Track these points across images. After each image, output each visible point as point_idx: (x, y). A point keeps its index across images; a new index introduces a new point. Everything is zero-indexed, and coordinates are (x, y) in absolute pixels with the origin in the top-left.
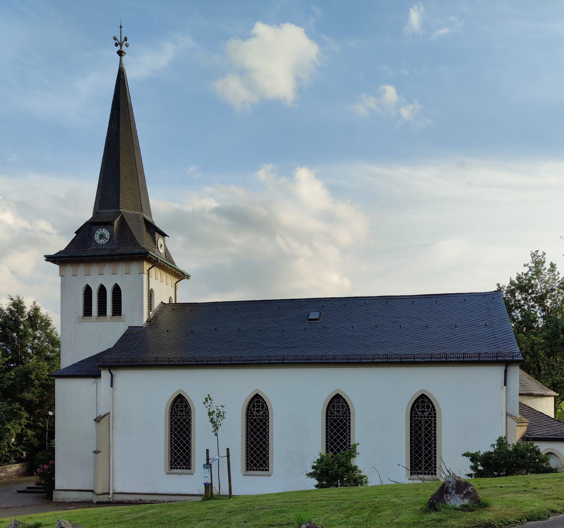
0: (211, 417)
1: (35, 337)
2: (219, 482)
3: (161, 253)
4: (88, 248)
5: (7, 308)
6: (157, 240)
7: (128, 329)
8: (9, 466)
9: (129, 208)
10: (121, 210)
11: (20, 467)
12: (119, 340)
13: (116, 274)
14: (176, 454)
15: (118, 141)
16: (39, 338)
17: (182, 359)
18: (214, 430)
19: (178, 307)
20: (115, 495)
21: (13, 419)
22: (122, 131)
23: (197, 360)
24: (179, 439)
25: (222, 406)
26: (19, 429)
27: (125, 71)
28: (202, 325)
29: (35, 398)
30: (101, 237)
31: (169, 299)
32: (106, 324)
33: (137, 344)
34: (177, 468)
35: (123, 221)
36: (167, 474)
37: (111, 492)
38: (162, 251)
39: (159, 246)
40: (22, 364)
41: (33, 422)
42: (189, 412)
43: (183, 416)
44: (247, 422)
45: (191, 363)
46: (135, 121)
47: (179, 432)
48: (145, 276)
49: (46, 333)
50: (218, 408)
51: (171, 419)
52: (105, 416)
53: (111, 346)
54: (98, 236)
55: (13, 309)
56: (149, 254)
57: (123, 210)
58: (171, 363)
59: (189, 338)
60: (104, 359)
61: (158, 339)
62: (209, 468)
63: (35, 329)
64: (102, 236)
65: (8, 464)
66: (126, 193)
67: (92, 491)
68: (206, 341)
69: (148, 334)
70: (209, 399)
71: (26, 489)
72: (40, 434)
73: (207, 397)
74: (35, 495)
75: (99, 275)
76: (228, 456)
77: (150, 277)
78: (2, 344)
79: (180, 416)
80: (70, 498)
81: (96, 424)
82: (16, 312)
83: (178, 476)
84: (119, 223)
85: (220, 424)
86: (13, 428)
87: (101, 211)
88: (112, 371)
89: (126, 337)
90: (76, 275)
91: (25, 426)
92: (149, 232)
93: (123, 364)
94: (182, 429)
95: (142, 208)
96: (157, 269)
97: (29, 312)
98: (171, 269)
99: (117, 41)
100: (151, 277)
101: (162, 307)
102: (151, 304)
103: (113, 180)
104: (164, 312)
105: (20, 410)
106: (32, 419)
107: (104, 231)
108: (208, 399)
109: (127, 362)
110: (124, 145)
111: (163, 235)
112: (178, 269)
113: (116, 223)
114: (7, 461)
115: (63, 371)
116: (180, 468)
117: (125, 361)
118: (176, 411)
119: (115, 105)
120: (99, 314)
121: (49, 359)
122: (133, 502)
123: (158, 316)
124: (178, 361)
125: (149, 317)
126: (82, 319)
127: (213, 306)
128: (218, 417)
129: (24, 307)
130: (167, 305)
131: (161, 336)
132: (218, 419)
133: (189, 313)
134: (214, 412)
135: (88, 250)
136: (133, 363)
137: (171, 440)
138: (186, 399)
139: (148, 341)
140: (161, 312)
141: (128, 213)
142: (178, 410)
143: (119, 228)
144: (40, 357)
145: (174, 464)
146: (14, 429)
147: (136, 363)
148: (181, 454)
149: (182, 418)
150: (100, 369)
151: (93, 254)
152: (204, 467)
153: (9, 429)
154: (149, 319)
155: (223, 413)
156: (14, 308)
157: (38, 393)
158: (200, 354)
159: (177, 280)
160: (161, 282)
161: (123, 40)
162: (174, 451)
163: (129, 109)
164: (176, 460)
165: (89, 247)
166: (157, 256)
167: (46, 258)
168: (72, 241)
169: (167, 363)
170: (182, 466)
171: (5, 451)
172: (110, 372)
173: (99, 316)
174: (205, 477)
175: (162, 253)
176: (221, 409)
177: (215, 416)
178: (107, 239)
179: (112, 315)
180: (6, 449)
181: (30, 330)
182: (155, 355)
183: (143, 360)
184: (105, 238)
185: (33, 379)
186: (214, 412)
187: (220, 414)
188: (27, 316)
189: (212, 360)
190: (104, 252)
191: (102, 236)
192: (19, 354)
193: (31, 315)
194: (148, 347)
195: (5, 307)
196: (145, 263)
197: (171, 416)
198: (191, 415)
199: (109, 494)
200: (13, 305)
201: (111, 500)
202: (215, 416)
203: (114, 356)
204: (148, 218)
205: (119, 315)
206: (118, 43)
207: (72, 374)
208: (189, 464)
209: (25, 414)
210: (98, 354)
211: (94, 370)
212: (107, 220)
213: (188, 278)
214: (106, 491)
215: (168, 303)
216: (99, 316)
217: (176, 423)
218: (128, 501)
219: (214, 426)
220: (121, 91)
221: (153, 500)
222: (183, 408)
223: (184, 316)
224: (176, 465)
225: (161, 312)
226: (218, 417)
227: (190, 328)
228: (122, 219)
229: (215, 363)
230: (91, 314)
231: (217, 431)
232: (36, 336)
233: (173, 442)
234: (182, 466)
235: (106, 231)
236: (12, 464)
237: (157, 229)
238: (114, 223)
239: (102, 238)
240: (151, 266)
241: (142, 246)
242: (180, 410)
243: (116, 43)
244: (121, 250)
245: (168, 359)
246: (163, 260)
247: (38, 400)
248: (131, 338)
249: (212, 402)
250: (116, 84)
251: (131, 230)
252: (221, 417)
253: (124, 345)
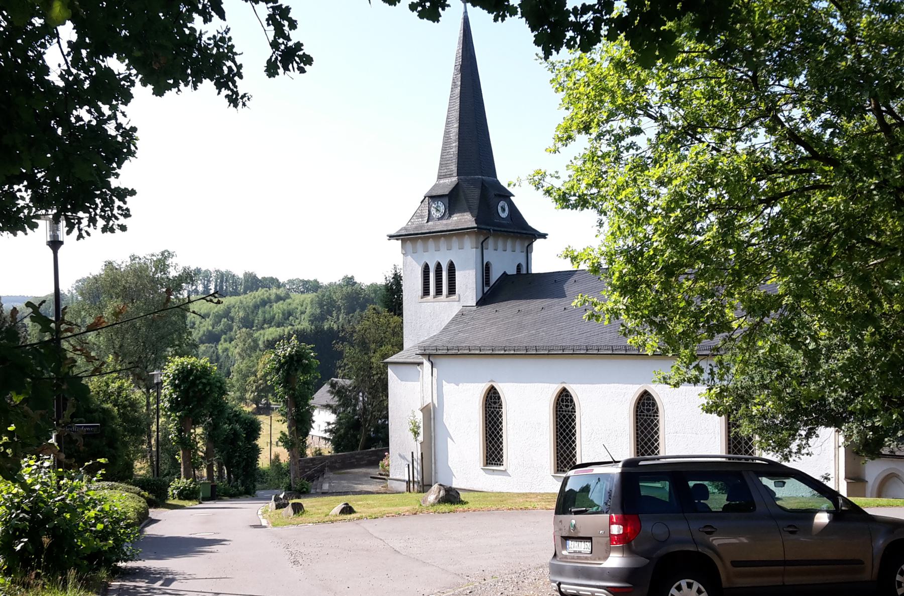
44: (557, 418)
164: (491, 455)
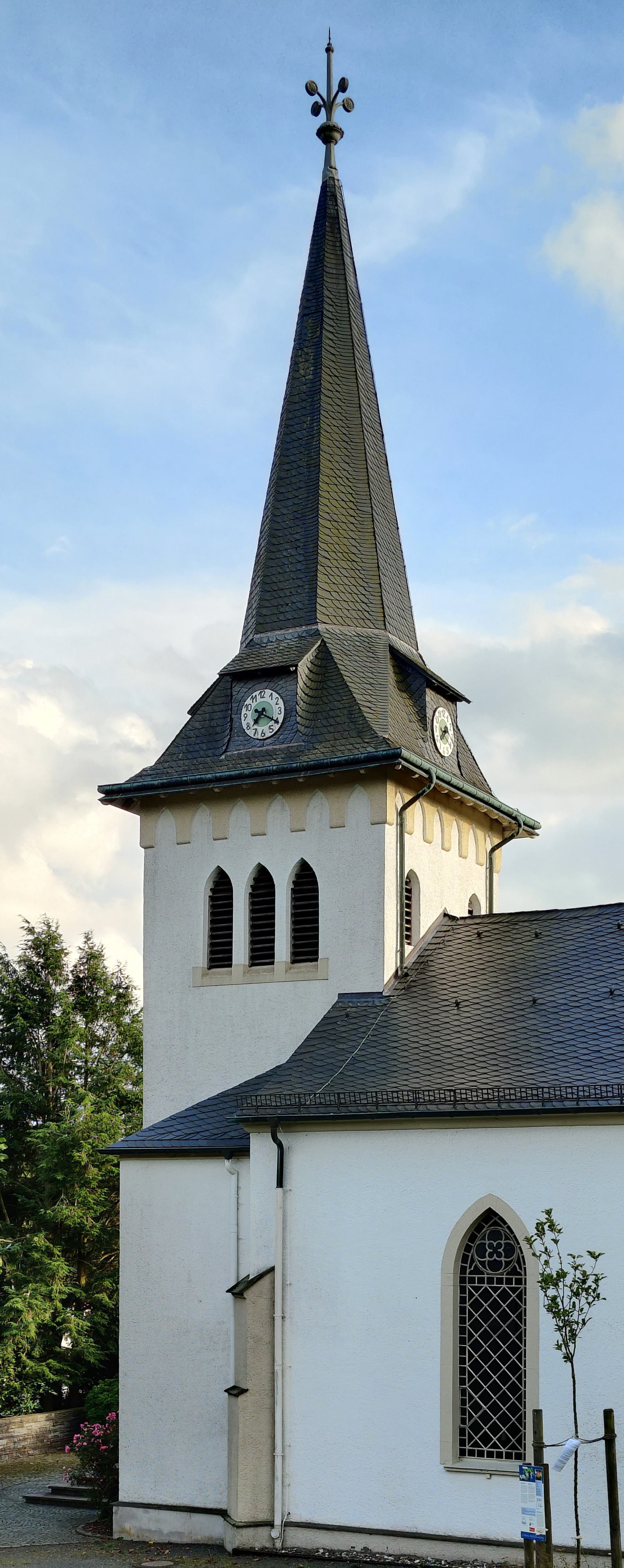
0: (551, 1292)
1: (92, 1041)
2: (578, 1534)
3: (442, 757)
4: (221, 755)
5: (20, 957)
6: (429, 713)
7: (337, 1002)
8: (17, 1419)
9: (347, 620)
10: (321, 627)
11: (48, 1423)
12: (308, 1039)
13: (304, 830)
14: (476, 1407)
15: (315, 412)
16: (103, 1043)
17: (496, 1094)
18: (561, 1342)
19: (496, 926)
20: (291, 1532)
21: (29, 1282)
22: (328, 378)
23: (546, 1096)
24: (486, 1357)
25: (594, 1256)
26: (45, 1310)
27: (340, 187)
28: (568, 982)
29: (90, 1219)
30: (259, 718)
31: (470, 903)
32: (272, 989)
33: (360, 1050)
34: (481, 1454)
35: (325, 658)
36: (449, 1470)
37: (278, 1522)
38: (446, 748)
39: (437, 733)
40: (59, 1119)
41: (86, 1292)
42: (520, 1268)
43: (500, 1281)
45: (525, 1106)
46: (370, 343)
47: (485, 1336)
48: (390, 832)
49: (118, 1026)
50: (579, 1261)
51: (463, 1290)
52: (260, 1277)
53: (284, 1059)
54: (249, 713)
55: (35, 959)
56: (400, 760)
57: (327, 626)
58: (460, 1108)
59: (524, 1025)
60: (259, 1098)
61: (426, 1031)
62: (539, 1479)
63: (92, 1016)
64: (261, 714)
65: (16, 1413)
66: (335, 570)
67: (223, 1513)
68: (580, 1034)
69: (396, 1016)
70: (549, 1226)
71: (49, 1494)
72: (104, 1325)
73: (543, 1218)
74: (70, 1512)
75: (253, 835)
76: (609, 1438)
77: (406, 836)
78: (7, 1061)
79: (490, 1281)
80: (160, 1532)
81: (235, 1303)
82: (42, 968)
83: (482, 1478)
84: (315, 670)
85: (583, 1320)
86: (29, 1307)
87: (262, 635)
88: (280, 1136)
89: (330, 1027)
90: (187, 840)
91: (62, 1301)
92: (403, 692)
93: (313, 1113)
94: (495, 1327)
95: (384, 616)
96: (432, 810)
97: (75, 966)
98: (475, 804)
99: (316, 98)
100: (411, 834)
101: (445, 928)
102: (408, 922)
103: (297, 537)
104: (450, 943)
105: (51, 1255)
106: (83, 1281)
107: (267, 699)
108: (546, 1227)
109: (327, 1106)
110: (334, 422)
111: (452, 697)
112: (496, 804)
113: (304, 668)
114: (12, 1405)
115: (142, 1138)
116: (490, 1455)
117: (321, 1103)
118: (476, 1266)
119: (308, 300)
120: (252, 958)
121: (129, 1103)
122: (343, 1555)
123: (431, 958)
124: (484, 1099)
125: (402, 961)
126: (203, 975)
127: (607, 916)
128: (577, 1294)
129: (62, 950)
130: (460, 922)
131: (437, 1022)
132: (577, 1301)
133: (530, 943)
134: (562, 1275)
135: (221, 761)
136: (343, 1109)
137: (462, 1361)
138: (509, 1228)
139: (394, 1039)
140: (441, 946)
141: (343, 634)
142: (483, 1263)
143: (313, 685)
144: (104, 1099)
145: (471, 1438)
146: (32, 1309)
147: (353, 1109)
148: (495, 1408)
149: (495, 1289)
150: (247, 1130)
151: (233, 773)
152: (523, 1477)
153: (19, 1312)
154: (401, 968)
155: (596, 1281)
156: (38, 955)
157: (97, 1203)
158: (556, 1077)
159: (497, 841)
160: (443, 849)
161: (335, 88)
162: (471, 1398)
163: (352, 306)
164: (476, 1428)
165: (225, 751)
166: (426, 765)
167: (104, 795)
168: (177, 736)
169: (449, 1106)
170: (495, 1446)
171: (9, 1375)
172: (275, 1139)
173: (252, 965)
174: (524, 1511)
175: (446, 755)
176: (588, 1264)
177: (564, 1292)
178: (277, 722)
179: (289, 961)
180: (11, 1371)
181: (80, 1021)
182: (414, 1084)
183: (374, 1099)
184: (272, 719)
185: (83, 1164)
186: (562, 1275)
187: (584, 1282)
188: (71, 977)
189: (596, 1094)
190: (267, 764)
191: (261, 714)
192: (51, 1090)
193: (81, 976)
194: (395, 1057)
195: (14, 954)
196: (390, 788)
197: (462, 1280)
198: (525, 1279)
199: (270, 1524)
200: (34, 948)
201: (278, 1545)
202: (564, 1292)
203: (290, 1087)
204: (403, 647)
205: (311, 961)
206: (322, 103)
207: (167, 1145)
208: (520, 1444)
209: (61, 1266)
210: (247, 1084)
211: (233, 1134)
212: (276, 661)
213: (531, 835)
214: (263, 1516)
215: (466, 915)
216: (252, 965)
217: (476, 1305)
218: (328, 1551)
219: (561, 1325)
220: (326, 255)
221: (405, 1555)
222: (499, 1255)
223: (511, 954)
224: (476, 1444)
225: (441, 946)
226: (577, 1294)
227: (529, 993)
228: (324, 654)
229: (603, 1104)
230: (230, 959)
231: (570, 1344)
232: (96, 1036)
233: (467, 1366)
234: (495, 1446)
235: (275, 695)
236: (26, 1413)
237: (432, 677)
238: (296, 669)
239: (261, 721)
240: (408, 797)
241: (380, 734)
242: (489, 1261)
243: (316, 103)
244: (319, 754)
245: (452, 1094)
246: (447, 777)
247: (98, 1225)
248: (343, 1029)
249: (560, 1237)
250: (313, 236)
251: (348, 686)
252: (588, 1294)
253: (322, 1052)
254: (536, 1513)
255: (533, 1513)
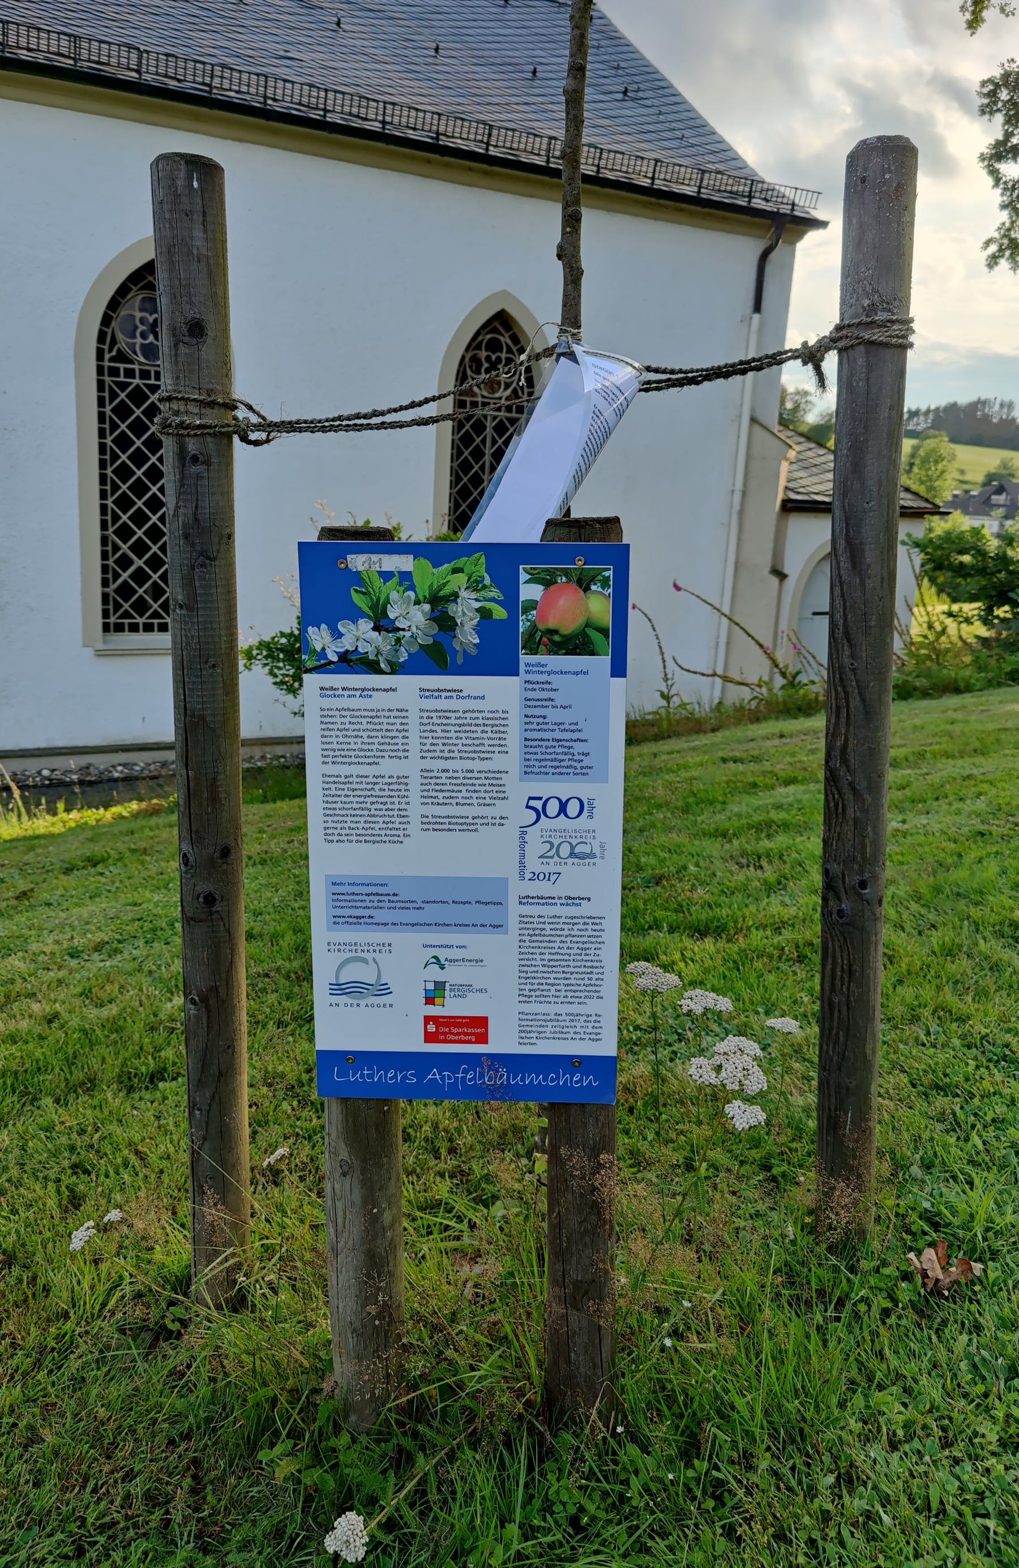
34: (134, 628)
224: (126, 615)
254: (514, 910)
255: (488, 914)
